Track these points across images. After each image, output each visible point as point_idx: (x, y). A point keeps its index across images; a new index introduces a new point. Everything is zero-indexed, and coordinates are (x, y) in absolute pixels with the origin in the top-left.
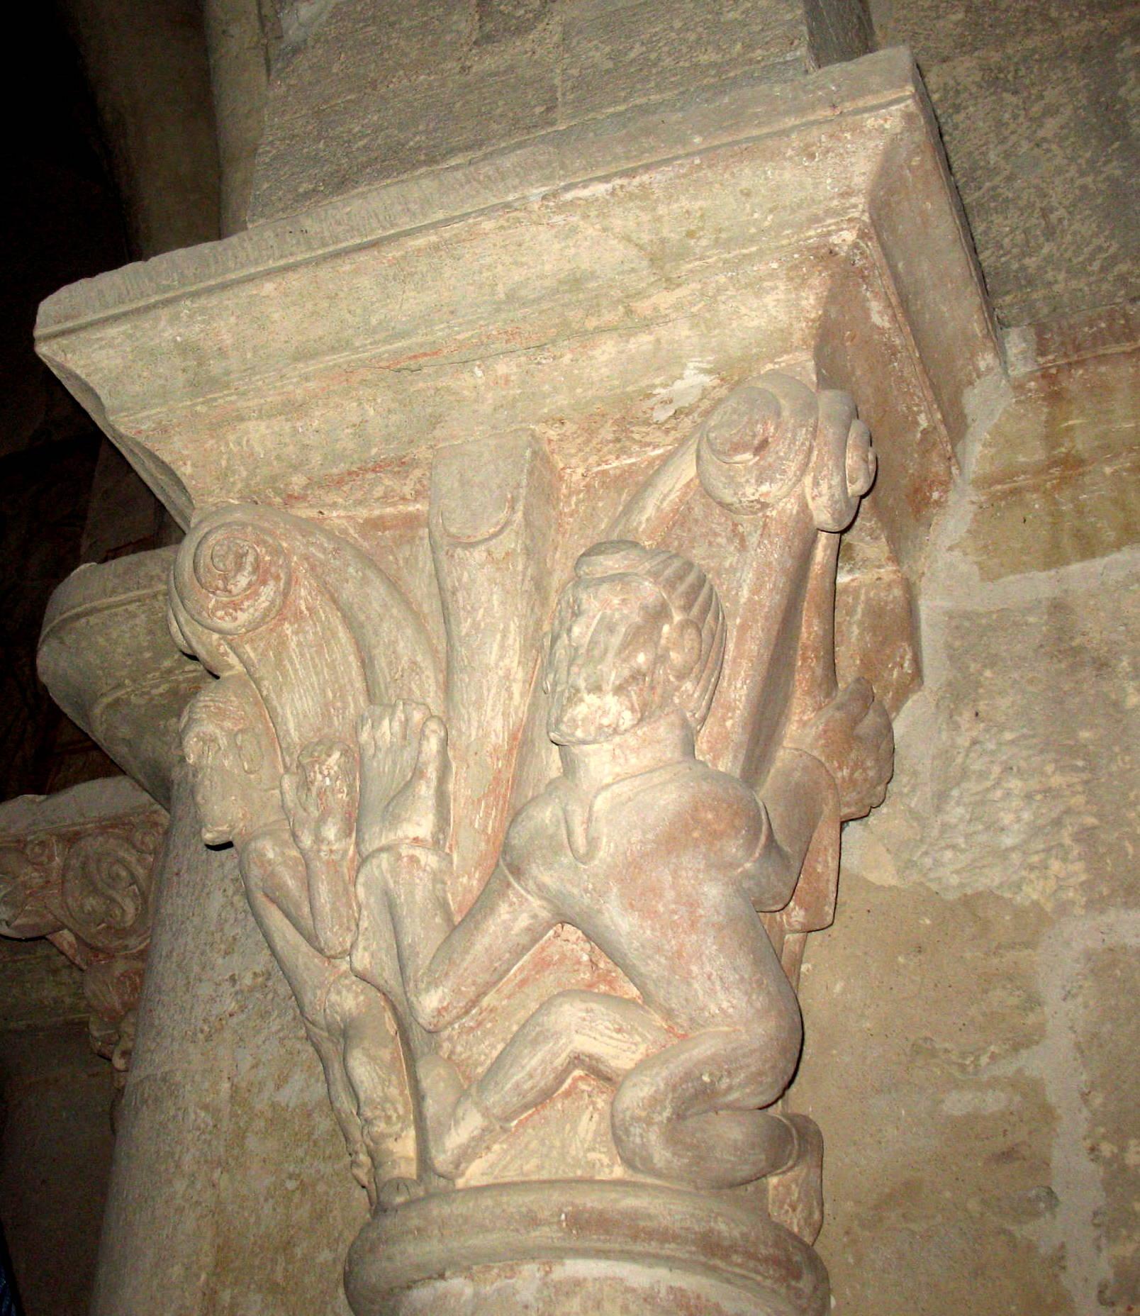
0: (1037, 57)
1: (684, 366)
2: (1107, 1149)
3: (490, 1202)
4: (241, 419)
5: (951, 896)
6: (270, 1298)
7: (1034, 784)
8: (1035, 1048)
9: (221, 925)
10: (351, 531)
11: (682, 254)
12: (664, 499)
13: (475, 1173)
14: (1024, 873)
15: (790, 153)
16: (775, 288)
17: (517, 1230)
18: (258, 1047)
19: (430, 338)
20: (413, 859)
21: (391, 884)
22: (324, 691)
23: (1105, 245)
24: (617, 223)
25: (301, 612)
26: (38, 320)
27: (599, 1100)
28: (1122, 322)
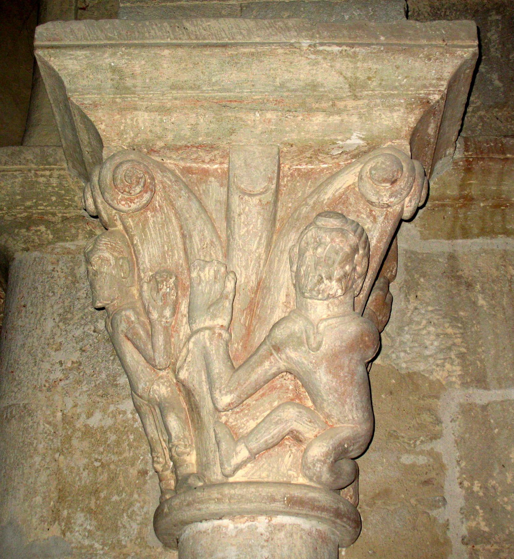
0: (454, 8)
1: (352, 135)
2: (466, 484)
3: (253, 490)
4: (136, 109)
5: (403, 372)
6: (88, 515)
7: (439, 331)
8: (438, 440)
9: (53, 336)
10: (177, 171)
11: (364, 87)
12: (337, 191)
13: (239, 476)
14: (434, 367)
15: (421, 55)
16: (399, 110)
17: (266, 503)
18: (76, 397)
19: (240, 95)
20: (220, 335)
21: (208, 344)
22: (163, 246)
23: (475, 101)
24: (338, 65)
25: (156, 207)
26: (36, 36)
27: (293, 449)
28: (500, 145)
